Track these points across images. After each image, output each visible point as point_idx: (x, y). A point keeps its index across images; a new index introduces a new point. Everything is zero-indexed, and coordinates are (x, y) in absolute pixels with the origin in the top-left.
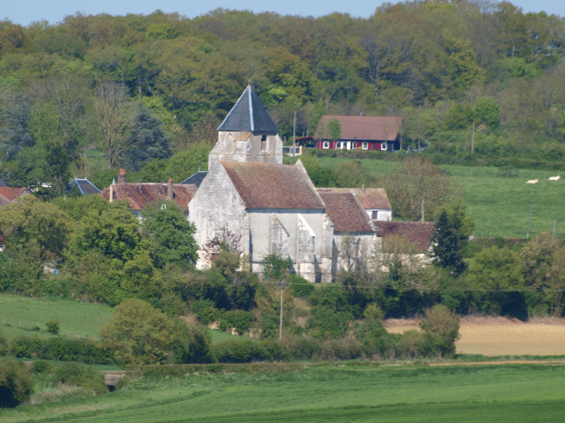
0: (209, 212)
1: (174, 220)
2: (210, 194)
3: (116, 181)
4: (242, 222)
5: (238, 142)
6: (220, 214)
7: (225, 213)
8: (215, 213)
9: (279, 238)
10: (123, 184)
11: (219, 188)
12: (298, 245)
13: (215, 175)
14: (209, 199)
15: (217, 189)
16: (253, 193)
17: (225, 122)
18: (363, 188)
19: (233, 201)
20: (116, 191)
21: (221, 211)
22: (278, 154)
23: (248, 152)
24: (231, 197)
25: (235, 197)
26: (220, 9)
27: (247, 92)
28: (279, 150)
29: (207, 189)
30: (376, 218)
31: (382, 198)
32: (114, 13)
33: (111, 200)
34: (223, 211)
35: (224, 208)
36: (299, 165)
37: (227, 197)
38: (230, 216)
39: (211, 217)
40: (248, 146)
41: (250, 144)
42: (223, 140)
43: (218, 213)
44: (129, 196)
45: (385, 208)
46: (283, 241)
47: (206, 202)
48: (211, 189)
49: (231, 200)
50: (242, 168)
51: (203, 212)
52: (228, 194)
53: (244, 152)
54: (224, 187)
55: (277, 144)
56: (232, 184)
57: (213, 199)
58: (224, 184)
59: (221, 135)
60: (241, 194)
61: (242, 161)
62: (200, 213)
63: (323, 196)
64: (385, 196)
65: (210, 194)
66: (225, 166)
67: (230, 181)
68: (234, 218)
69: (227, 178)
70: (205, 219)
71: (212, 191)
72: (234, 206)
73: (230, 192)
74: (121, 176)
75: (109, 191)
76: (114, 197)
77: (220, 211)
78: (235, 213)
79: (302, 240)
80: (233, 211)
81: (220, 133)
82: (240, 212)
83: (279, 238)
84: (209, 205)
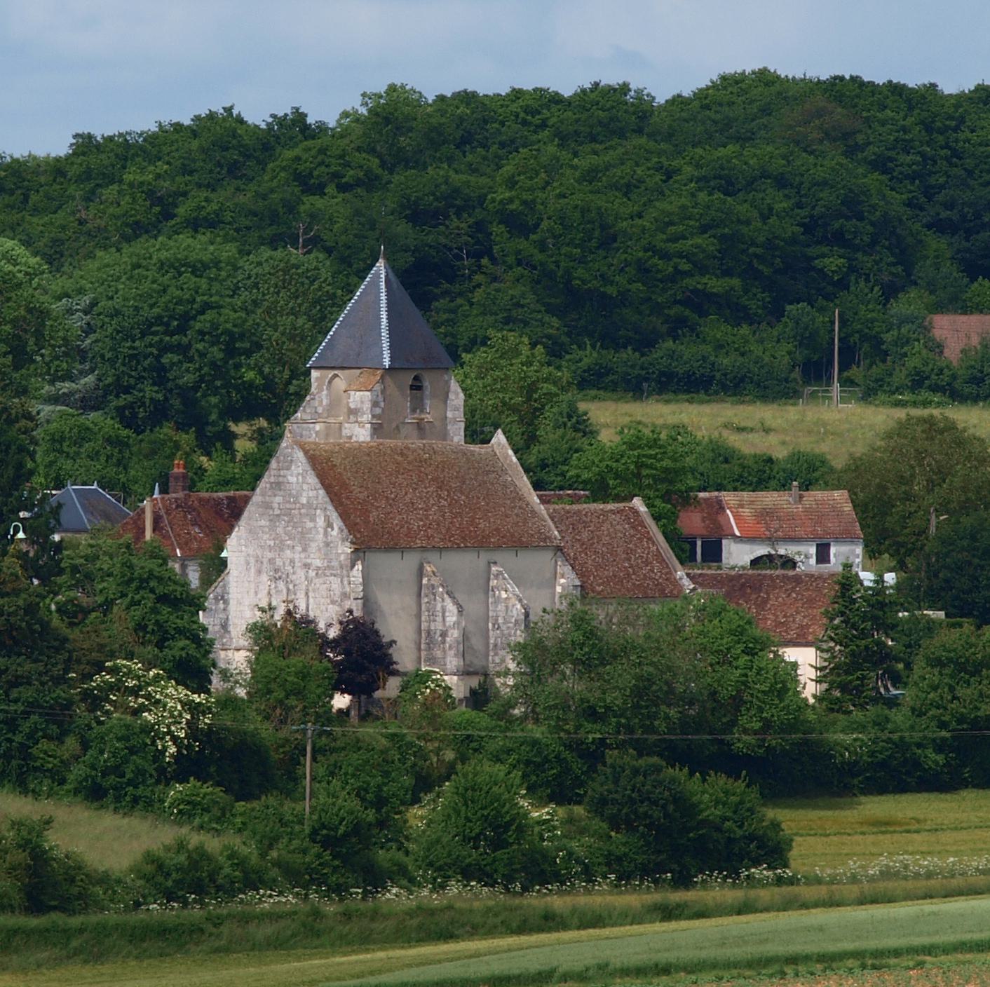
0: (271, 561)
1: (153, 584)
2: (274, 519)
3: (164, 491)
4: (345, 580)
5: (352, 393)
6: (298, 564)
7: (309, 561)
8: (287, 563)
9: (439, 619)
10: (181, 495)
11: (295, 503)
12: (491, 633)
13: (282, 473)
14: (272, 528)
15: (288, 506)
16: (373, 516)
17: (833, 340)
18: (795, 491)
19: (326, 533)
20: (162, 512)
21: (298, 556)
22: (455, 421)
23: (373, 416)
24: (321, 522)
25: (330, 525)
26: (765, 69)
27: (377, 275)
28: (456, 409)
29: (268, 506)
30: (828, 561)
31: (840, 513)
32: (790, 67)
33: (148, 534)
34: (303, 556)
35: (304, 550)
36: (499, 444)
37: (310, 525)
38: (318, 568)
39: (276, 571)
40: (375, 404)
41: (381, 399)
42: (320, 389)
43: (292, 561)
44: (195, 524)
45: (845, 537)
46: (447, 624)
48: (276, 505)
49: (321, 531)
50: (356, 454)
51: (259, 561)
52: (313, 520)
53: (367, 417)
54: (304, 500)
55: (451, 396)
56: (322, 492)
57: (280, 530)
58: (305, 494)
59: (317, 379)
60: (344, 516)
61: (362, 439)
62: (252, 561)
63: (556, 519)
64: (848, 508)
65: (274, 519)
66: (306, 452)
67: (319, 485)
68: (328, 572)
69: (312, 480)
70: (264, 578)
71: (277, 512)
72: (327, 544)
73: (318, 511)
74: (177, 478)
75: (143, 511)
76: (156, 527)
77: (297, 556)
78: (330, 561)
79: (500, 620)
80: (326, 557)
81: (315, 374)
82: (342, 558)
83: (439, 619)
84: (272, 543)
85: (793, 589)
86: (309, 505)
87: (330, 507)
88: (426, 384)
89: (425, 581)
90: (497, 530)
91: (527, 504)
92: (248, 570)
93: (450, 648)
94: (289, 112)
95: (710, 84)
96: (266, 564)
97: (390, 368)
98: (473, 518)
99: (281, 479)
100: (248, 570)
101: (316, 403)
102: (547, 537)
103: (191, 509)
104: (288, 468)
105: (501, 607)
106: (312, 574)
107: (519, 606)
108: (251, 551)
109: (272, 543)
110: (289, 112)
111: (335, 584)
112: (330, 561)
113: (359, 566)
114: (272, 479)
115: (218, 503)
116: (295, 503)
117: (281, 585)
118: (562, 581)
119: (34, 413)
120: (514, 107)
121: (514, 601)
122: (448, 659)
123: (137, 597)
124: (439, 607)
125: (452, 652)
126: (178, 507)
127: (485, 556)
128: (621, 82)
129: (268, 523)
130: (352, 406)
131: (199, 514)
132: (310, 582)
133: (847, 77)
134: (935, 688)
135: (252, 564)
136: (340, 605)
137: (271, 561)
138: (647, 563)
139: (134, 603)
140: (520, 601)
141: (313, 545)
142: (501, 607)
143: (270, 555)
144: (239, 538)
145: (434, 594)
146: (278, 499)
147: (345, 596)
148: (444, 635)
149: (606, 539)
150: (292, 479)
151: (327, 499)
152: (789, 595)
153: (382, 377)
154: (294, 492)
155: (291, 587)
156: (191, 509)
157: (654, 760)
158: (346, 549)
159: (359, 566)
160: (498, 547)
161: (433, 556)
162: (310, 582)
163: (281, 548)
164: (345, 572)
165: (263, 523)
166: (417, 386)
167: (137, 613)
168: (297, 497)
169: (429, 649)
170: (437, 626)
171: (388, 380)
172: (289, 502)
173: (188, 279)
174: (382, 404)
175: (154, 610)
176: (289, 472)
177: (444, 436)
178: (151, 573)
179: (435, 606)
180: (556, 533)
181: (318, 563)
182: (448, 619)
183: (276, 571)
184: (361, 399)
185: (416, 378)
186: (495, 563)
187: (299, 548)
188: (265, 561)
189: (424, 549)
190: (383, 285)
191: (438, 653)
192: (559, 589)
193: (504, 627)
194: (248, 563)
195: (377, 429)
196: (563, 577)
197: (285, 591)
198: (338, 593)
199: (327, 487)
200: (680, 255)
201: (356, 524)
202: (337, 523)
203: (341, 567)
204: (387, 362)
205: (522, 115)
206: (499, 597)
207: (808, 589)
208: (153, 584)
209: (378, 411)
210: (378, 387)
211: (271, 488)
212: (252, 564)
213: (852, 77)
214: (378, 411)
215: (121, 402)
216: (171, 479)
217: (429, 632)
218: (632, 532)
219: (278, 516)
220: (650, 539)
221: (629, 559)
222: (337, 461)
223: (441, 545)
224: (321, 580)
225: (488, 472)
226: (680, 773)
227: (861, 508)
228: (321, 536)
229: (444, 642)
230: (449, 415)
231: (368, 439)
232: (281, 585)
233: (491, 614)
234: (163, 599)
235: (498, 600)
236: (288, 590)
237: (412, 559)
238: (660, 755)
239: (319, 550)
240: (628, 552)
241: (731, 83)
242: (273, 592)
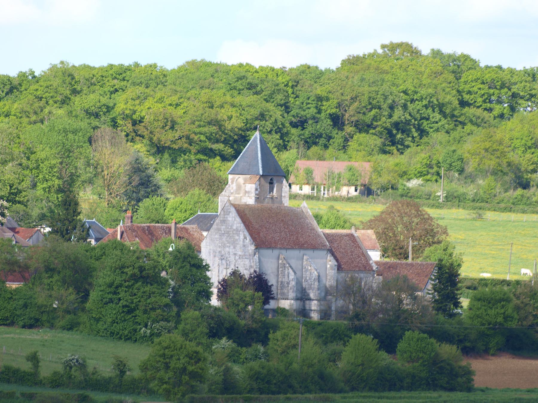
0: (220, 252)
2: (222, 235)
4: (251, 261)
6: (231, 253)
7: (236, 252)
8: (227, 253)
9: (286, 277)
15: (228, 230)
16: (261, 234)
19: (244, 241)
21: (231, 250)
24: (242, 237)
25: (245, 238)
29: (219, 230)
35: (234, 248)
37: (237, 237)
39: (222, 256)
40: (256, 190)
41: (258, 187)
42: (232, 183)
43: (229, 253)
47: (217, 242)
48: (222, 229)
49: (242, 240)
52: (238, 235)
55: (284, 187)
56: (242, 225)
57: (224, 239)
58: (235, 225)
60: (251, 235)
62: (212, 252)
64: (374, 237)
65: (222, 235)
66: (235, 208)
67: (241, 222)
68: (244, 257)
69: (238, 219)
70: (217, 259)
71: (223, 232)
72: (244, 246)
73: (241, 232)
77: (231, 250)
79: (308, 278)
82: (250, 251)
83: (286, 277)
86: (237, 230)
87: (246, 231)
88: (275, 182)
89: (280, 262)
92: (210, 255)
94: (27, 71)
96: (217, 254)
97: (262, 176)
98: (297, 237)
100: (210, 255)
101: (231, 188)
104: (228, 214)
105: (308, 273)
106: (237, 258)
107: (316, 273)
108: (211, 248)
110: (27, 71)
111: (247, 262)
112: (245, 253)
113: (257, 255)
114: (221, 219)
115: (143, 228)
116: (231, 229)
117: (224, 262)
118: (330, 263)
119: (531, 184)
121: (313, 270)
122: (290, 293)
124: (286, 273)
125: (291, 291)
127: (302, 252)
130: (247, 190)
132: (236, 261)
133: (245, 64)
134: (478, 309)
135: (211, 253)
136: (249, 271)
139: (182, 267)
140: (316, 270)
141: (238, 246)
143: (219, 249)
144: (206, 243)
145: (285, 267)
146: (223, 227)
147: (251, 267)
148: (288, 283)
149: (343, 247)
150: (230, 219)
151: (244, 228)
153: (259, 179)
154: (230, 224)
155: (228, 262)
156: (134, 231)
157: (426, 335)
158: (252, 248)
159: (257, 255)
160: (307, 249)
161: (284, 252)
162: (236, 261)
163: (224, 246)
164: (251, 257)
165: (217, 236)
166: (271, 183)
167: (182, 271)
168: (232, 226)
169: (282, 289)
170: (285, 280)
173: (71, 136)
174: (259, 190)
176: (228, 216)
178: (189, 255)
179: (285, 272)
180: (328, 243)
181: (240, 253)
182: (290, 277)
183: (222, 256)
184: (251, 187)
185: (271, 179)
186: (306, 255)
187: (232, 247)
188: (217, 252)
189: (280, 248)
190: (258, 142)
192: (328, 266)
193: (309, 281)
194: (210, 253)
195: (257, 199)
196: (330, 261)
197: (225, 264)
198: (248, 265)
200: (201, 133)
201: (256, 238)
202: (249, 238)
203: (250, 255)
205: (115, 75)
206: (307, 269)
208: (189, 259)
210: (258, 183)
211: (221, 222)
212: (211, 253)
213: (247, 63)
215: (45, 185)
218: (353, 244)
219: (223, 234)
222: (247, 212)
224: (241, 260)
225: (301, 219)
226: (433, 340)
228: (241, 243)
229: (288, 286)
230: (283, 195)
231: (254, 203)
232: (224, 262)
234: (194, 265)
235: (307, 270)
236: (227, 264)
237: (276, 252)
238: (428, 334)
239: (241, 248)
240: (352, 252)
242: (220, 264)
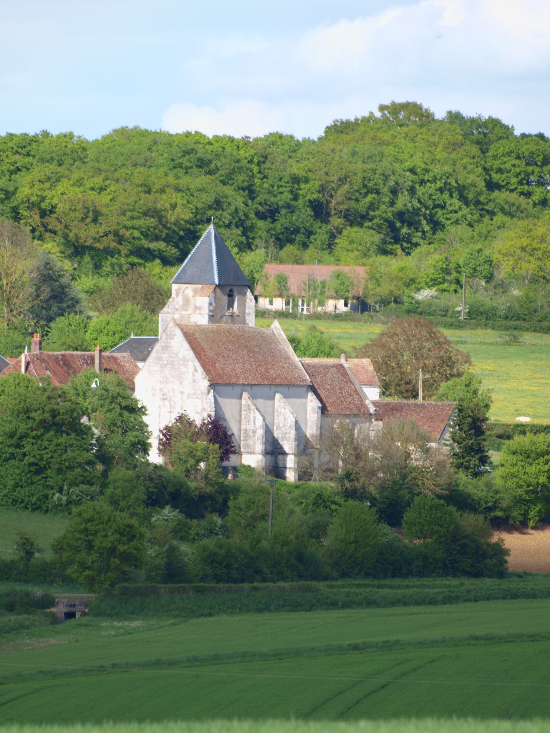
0: (161, 390)
1: (120, 399)
2: (163, 366)
4: (204, 401)
13: (169, 341)
15: (172, 359)
16: (217, 365)
19: (194, 375)
25: (196, 370)
27: (209, 233)
29: (160, 359)
35: (181, 383)
36: (276, 328)
39: (164, 395)
40: (210, 304)
42: (177, 295)
48: (164, 359)
56: (191, 353)
60: (203, 366)
64: (371, 368)
65: (163, 366)
68: (194, 397)
69: (186, 345)
71: (166, 362)
72: (194, 381)
83: (252, 423)
85: (421, 411)
88: (235, 293)
90: (279, 375)
91: (292, 362)
93: (258, 439)
95: (510, 126)
99: (168, 344)
101: (175, 303)
102: (303, 380)
103: (43, 361)
105: (282, 418)
106: (185, 397)
109: (162, 380)
115: (56, 357)
117: (166, 402)
120: (11, 144)
123: (110, 407)
124: (252, 418)
126: (37, 359)
128: (69, 131)
129: (160, 369)
131: (48, 363)
137: (161, 390)
138: (351, 395)
139: (110, 411)
142: (282, 418)
145: (249, 410)
147: (204, 409)
148: (254, 432)
152: (419, 414)
153: (215, 289)
154: (175, 352)
155: (172, 404)
156: (43, 361)
170: (251, 427)
171: (218, 290)
172: (172, 357)
174: (214, 304)
175: (121, 415)
177: (244, 322)
183: (164, 395)
185: (231, 291)
190: (213, 239)
191: (251, 442)
195: (212, 318)
197: (169, 406)
199: (194, 349)
200: (134, 228)
202: (200, 369)
203: (202, 394)
204: (217, 281)
205: (16, 148)
207: (429, 412)
209: (212, 308)
214: (212, 308)
216: (33, 344)
217: (246, 430)
218: (342, 378)
220: (351, 382)
221: (341, 393)
223: (253, 382)
227: (378, 368)
229: (254, 436)
230: (247, 311)
233: (275, 421)
236: (171, 406)
240: (341, 388)
241: (123, 132)
